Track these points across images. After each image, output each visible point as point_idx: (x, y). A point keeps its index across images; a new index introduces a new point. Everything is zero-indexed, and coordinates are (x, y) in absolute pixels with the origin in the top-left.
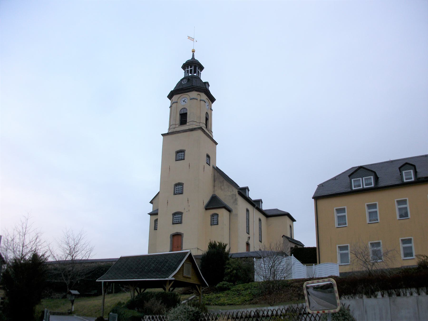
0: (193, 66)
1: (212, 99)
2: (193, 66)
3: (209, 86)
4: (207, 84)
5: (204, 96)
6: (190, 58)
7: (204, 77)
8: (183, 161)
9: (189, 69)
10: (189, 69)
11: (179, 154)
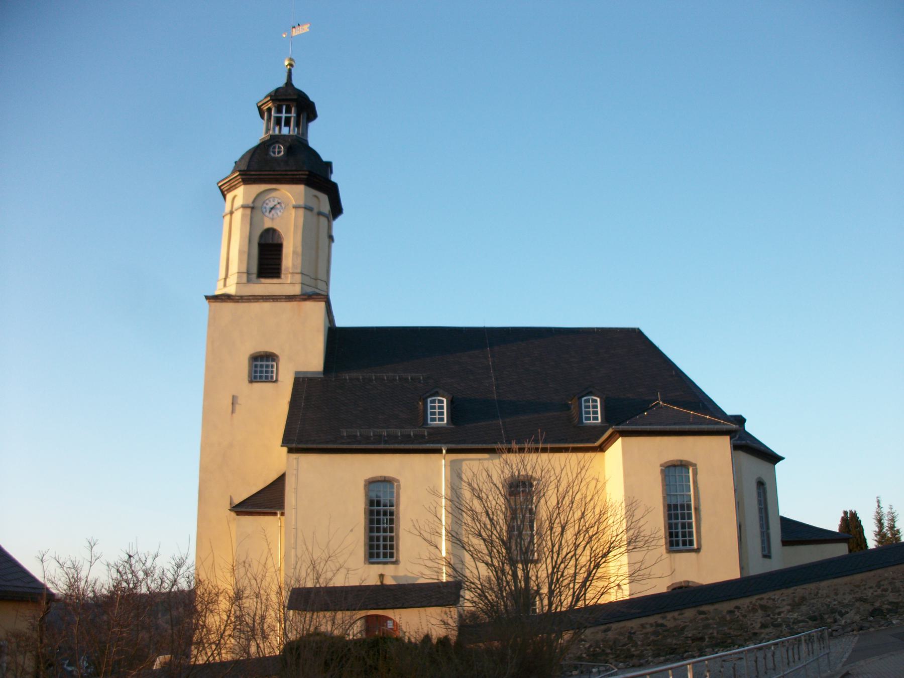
0: (292, 104)
1: (336, 209)
2: (292, 104)
3: (331, 172)
4: (329, 165)
5: (326, 207)
6: (281, 82)
7: (319, 137)
8: (693, 555)
9: (284, 115)
10: (284, 115)
11: (259, 363)
